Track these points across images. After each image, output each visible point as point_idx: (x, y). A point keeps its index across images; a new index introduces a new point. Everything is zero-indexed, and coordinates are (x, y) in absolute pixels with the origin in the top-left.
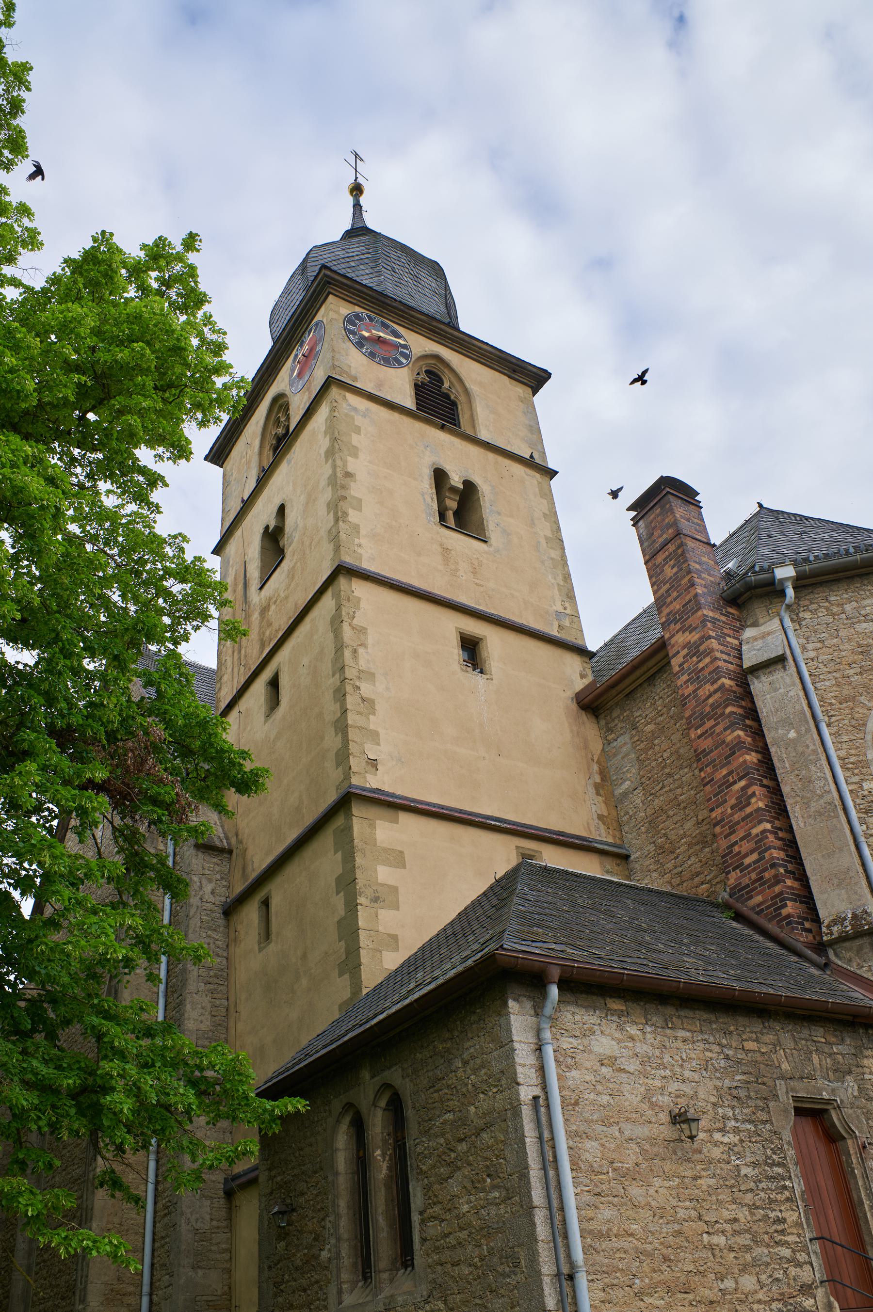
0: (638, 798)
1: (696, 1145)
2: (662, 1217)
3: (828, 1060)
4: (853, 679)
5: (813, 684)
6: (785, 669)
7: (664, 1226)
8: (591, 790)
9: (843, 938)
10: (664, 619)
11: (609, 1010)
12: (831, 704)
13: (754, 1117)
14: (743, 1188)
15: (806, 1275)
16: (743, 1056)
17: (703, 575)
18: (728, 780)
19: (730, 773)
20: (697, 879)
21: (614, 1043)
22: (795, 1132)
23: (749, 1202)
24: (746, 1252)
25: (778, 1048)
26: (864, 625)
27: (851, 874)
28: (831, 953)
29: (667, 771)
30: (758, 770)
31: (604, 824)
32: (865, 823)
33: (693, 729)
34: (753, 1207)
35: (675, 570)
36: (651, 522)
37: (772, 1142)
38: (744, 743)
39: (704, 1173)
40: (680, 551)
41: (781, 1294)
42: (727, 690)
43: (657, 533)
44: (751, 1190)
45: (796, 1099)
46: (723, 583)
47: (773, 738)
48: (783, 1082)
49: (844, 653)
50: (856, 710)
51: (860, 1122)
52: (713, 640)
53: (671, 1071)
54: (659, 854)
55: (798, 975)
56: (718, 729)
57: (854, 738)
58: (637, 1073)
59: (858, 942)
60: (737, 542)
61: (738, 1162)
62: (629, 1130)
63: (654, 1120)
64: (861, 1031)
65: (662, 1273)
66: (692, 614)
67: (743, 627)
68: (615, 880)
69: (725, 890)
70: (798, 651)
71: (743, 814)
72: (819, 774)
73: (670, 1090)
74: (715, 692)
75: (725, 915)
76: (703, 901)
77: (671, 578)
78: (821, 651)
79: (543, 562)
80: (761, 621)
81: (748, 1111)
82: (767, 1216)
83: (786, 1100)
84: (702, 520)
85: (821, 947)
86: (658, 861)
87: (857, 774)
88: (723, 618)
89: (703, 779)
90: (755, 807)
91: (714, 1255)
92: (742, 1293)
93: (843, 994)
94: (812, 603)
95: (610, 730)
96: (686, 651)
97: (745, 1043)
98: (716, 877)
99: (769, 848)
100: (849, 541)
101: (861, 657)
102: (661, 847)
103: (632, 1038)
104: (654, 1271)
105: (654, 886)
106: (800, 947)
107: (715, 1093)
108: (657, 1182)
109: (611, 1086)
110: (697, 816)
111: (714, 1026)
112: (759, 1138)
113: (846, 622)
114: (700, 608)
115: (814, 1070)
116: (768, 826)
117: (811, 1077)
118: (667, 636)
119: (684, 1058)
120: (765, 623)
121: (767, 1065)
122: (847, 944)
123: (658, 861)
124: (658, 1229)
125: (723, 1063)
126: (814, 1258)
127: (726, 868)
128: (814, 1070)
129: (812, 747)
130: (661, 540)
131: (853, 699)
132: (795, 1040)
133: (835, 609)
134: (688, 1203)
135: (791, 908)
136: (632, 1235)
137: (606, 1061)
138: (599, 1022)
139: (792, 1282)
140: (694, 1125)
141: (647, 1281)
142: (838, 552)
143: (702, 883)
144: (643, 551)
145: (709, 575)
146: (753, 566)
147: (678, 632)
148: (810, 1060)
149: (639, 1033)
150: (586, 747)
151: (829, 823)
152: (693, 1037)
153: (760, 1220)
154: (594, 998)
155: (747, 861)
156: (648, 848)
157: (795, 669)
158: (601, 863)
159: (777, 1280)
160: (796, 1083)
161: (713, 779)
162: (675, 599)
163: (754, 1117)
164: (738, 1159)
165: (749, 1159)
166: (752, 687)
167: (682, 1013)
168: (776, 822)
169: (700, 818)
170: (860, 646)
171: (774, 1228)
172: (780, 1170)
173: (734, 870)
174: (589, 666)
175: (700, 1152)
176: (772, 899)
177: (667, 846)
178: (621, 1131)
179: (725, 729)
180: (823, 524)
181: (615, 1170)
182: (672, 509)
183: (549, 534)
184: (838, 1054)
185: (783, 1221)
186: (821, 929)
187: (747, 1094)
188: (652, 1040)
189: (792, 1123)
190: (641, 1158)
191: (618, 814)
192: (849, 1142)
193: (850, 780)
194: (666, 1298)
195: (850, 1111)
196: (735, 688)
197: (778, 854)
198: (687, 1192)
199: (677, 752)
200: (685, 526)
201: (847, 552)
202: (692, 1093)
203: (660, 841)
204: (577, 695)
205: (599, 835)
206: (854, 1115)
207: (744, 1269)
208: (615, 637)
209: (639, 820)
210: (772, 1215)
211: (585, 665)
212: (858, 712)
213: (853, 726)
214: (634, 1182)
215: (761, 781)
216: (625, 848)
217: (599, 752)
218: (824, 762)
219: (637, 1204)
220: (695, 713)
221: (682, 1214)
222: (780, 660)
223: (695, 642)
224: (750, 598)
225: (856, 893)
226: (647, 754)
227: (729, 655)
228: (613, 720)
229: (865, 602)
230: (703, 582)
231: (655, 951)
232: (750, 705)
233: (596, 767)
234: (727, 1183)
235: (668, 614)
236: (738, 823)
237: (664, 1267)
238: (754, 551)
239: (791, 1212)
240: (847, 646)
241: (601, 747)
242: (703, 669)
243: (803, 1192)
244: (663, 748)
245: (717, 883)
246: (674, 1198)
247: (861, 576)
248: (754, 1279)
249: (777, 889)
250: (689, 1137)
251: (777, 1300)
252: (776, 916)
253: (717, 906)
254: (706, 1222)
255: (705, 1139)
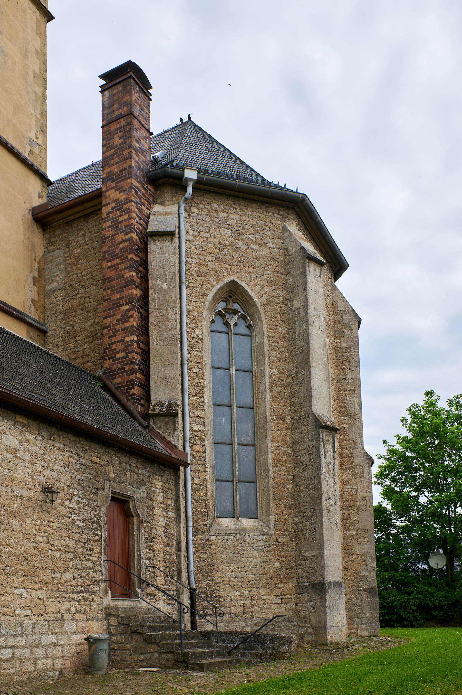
0: (60, 296)
1: (54, 506)
2: (27, 539)
3: (135, 476)
4: (209, 264)
5: (186, 258)
6: (172, 242)
7: (28, 543)
8: (30, 281)
9: (160, 414)
10: (105, 175)
11: (17, 421)
12: (192, 275)
13: (89, 497)
14: (75, 531)
15: (98, 576)
16: (90, 464)
17: (139, 153)
18: (119, 302)
19: (122, 298)
20: (86, 359)
21: (17, 441)
22: (109, 509)
23: (77, 539)
24: (70, 562)
25: (110, 464)
26: (226, 231)
27: (174, 380)
28: (151, 421)
29: (83, 284)
30: (139, 302)
31: (34, 306)
32: (190, 353)
33: (106, 261)
34: (78, 541)
35: (121, 141)
36: (114, 95)
37: (95, 511)
38: (135, 281)
39: (55, 520)
40: (128, 128)
41: (83, 583)
42: (134, 243)
43: (116, 106)
44: (79, 533)
45: (113, 492)
46: (150, 165)
47: (153, 284)
48: (108, 483)
49: (209, 245)
50: (205, 284)
51: (143, 510)
52: (133, 204)
53: (48, 464)
54: (66, 336)
55: (131, 428)
56: (122, 266)
57: (198, 300)
58: (27, 461)
59: (167, 419)
60: (167, 138)
61: (75, 518)
62: (17, 491)
63: (32, 488)
64: (156, 465)
65: (23, 566)
66: (125, 180)
67: (154, 203)
68: (35, 344)
69: (101, 370)
70: (183, 232)
71: (123, 326)
72: (173, 316)
73: (45, 474)
74: (126, 240)
75: (98, 384)
76: (87, 373)
77: (117, 146)
78: (196, 238)
79: (28, 93)
80: (167, 203)
81: (86, 493)
82: (84, 547)
83: (108, 491)
84: (149, 110)
85: (147, 416)
86: (65, 340)
87: (194, 323)
88: (144, 191)
89: (104, 297)
90: (131, 324)
91: (52, 561)
92: (64, 580)
93: (152, 444)
94: (201, 203)
95: (51, 243)
96: (113, 205)
97: (93, 458)
98: (97, 360)
99: (133, 352)
100: (235, 170)
101: (218, 251)
102: (68, 332)
103: (28, 441)
104: (18, 564)
105: (59, 356)
106: (135, 413)
107: (70, 480)
108: (28, 521)
109: (11, 465)
110: (95, 320)
111: (78, 445)
112: (89, 508)
113: (216, 224)
114: (130, 177)
115: (126, 480)
116: (136, 338)
117: (123, 483)
118: (104, 189)
119: (57, 458)
120: (169, 205)
121: (102, 472)
122: (161, 418)
123: (65, 340)
124: (25, 544)
125: (78, 466)
126: (103, 569)
127: (105, 356)
128: (126, 480)
129: (174, 298)
130: (117, 113)
131: (204, 276)
132: (120, 462)
133: (213, 213)
134: (43, 534)
135: (136, 390)
136: (9, 545)
137: (10, 451)
138: (10, 427)
139: (90, 579)
140: (55, 495)
141: (13, 568)
142: (226, 174)
143: (88, 362)
144: (103, 116)
145: (143, 155)
146: (172, 161)
147: (112, 189)
148: (126, 474)
149: (33, 439)
150: (32, 249)
151: (170, 347)
152: (64, 448)
153: (80, 548)
154: (9, 412)
155: (118, 356)
156: (60, 330)
157: (178, 244)
158: (28, 332)
159: (83, 577)
160: (115, 484)
161: (110, 299)
162: (116, 164)
163: (89, 497)
164: (75, 516)
165: (82, 517)
166: (149, 246)
167: (61, 434)
168: (141, 337)
169: (96, 321)
170: (220, 243)
171: (87, 552)
172: (96, 526)
173: (109, 359)
174: (46, 191)
175: (55, 509)
176: (127, 382)
177: (72, 333)
178: (12, 491)
179: (126, 268)
180: (224, 150)
181: (5, 510)
182: (131, 92)
183: (37, 71)
184: (141, 474)
185: (93, 550)
186: (149, 406)
187: (88, 484)
188: (40, 445)
189: (108, 504)
190: (21, 507)
191: (45, 303)
192: (135, 518)
193: (189, 326)
194: (23, 578)
195: (140, 504)
196: (138, 243)
197: (137, 357)
198: (44, 528)
199: (92, 273)
200: (136, 107)
201: (232, 175)
202: (57, 478)
203: (68, 328)
204: (34, 209)
205: (30, 313)
206: (141, 506)
207: (67, 570)
208: (69, 176)
209: (58, 311)
210: (87, 546)
211: (43, 188)
212: (206, 285)
213: (200, 293)
214: (15, 518)
215: (139, 309)
216: (45, 326)
217: (41, 256)
218: (178, 310)
219: (14, 530)
220: (109, 251)
221: (39, 538)
222: (170, 234)
223: (121, 201)
224: (164, 184)
225: (174, 391)
226: (72, 268)
227: (141, 219)
228: (55, 237)
229: (232, 216)
230: (137, 159)
231: (52, 394)
232: (144, 258)
233: (36, 266)
234: (67, 527)
235: (109, 173)
236: (118, 331)
237: (24, 563)
238: (176, 151)
239: (97, 547)
240: (212, 241)
241: (42, 253)
242: (122, 222)
243: (106, 538)
244: (83, 267)
245: (98, 364)
246: (36, 530)
247: (245, 199)
248: (71, 575)
249: (131, 377)
250: (51, 501)
251: (81, 586)
252: (127, 393)
253: (94, 377)
254: (52, 545)
255: (60, 503)
